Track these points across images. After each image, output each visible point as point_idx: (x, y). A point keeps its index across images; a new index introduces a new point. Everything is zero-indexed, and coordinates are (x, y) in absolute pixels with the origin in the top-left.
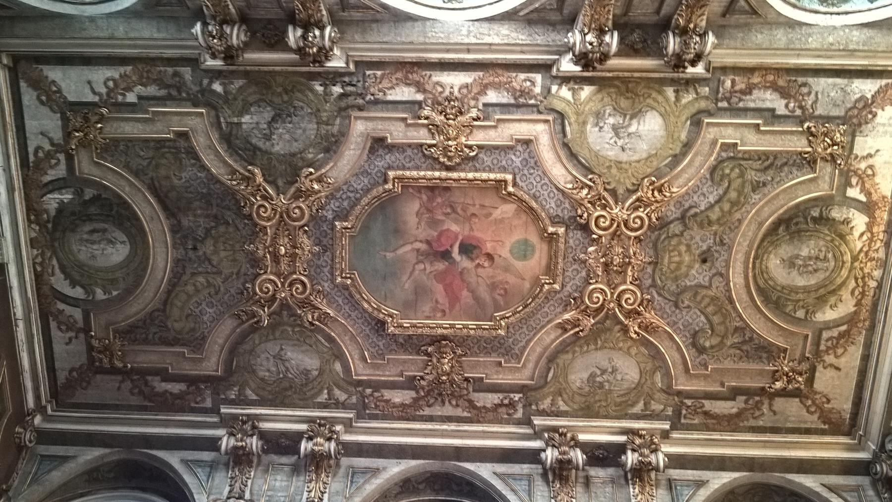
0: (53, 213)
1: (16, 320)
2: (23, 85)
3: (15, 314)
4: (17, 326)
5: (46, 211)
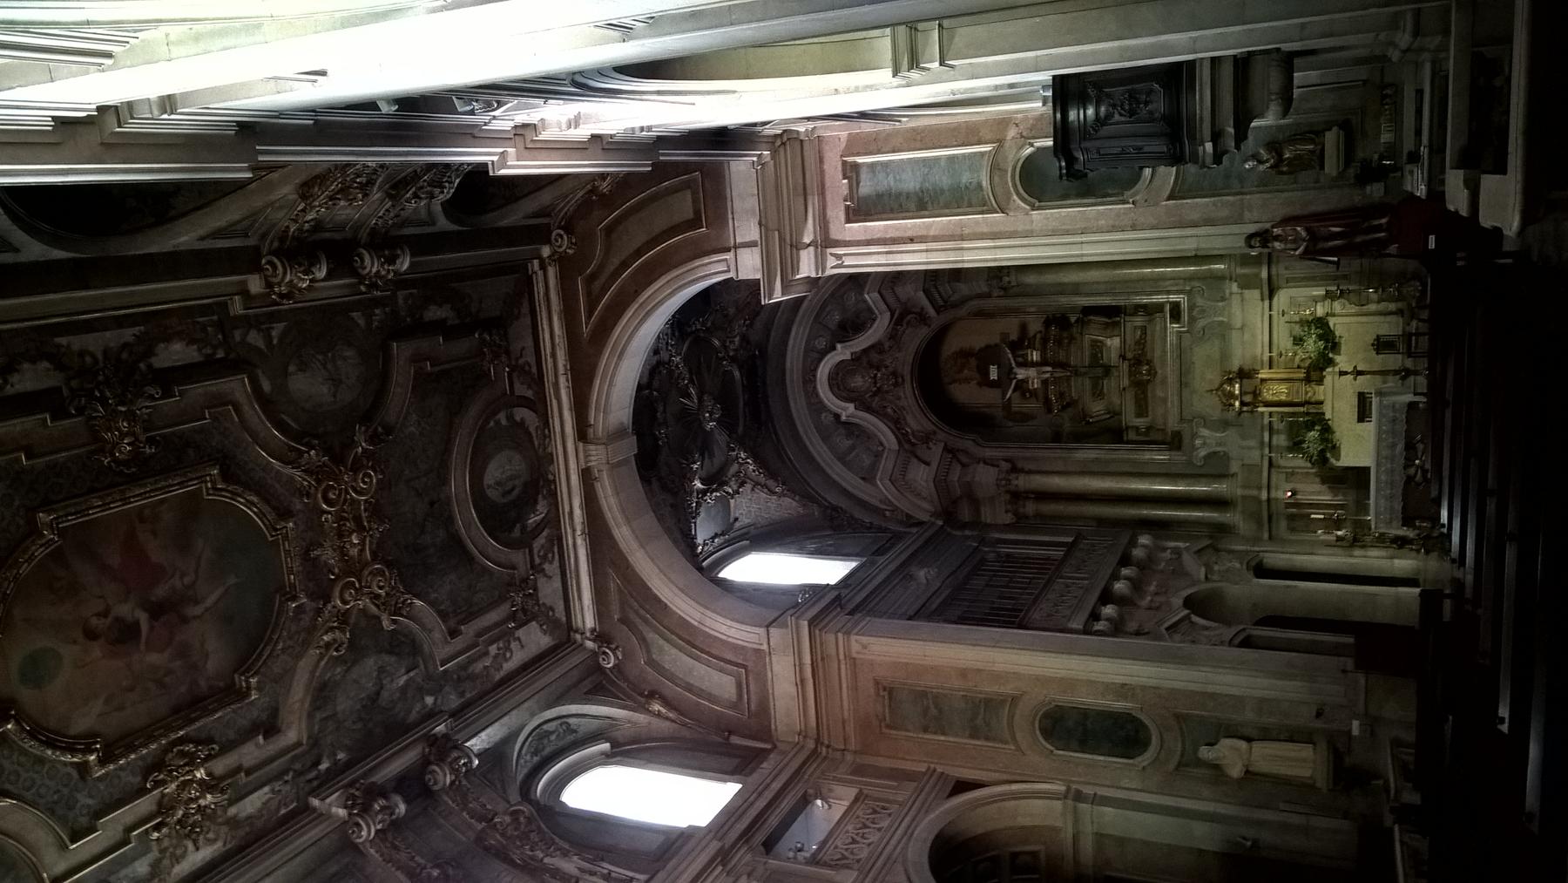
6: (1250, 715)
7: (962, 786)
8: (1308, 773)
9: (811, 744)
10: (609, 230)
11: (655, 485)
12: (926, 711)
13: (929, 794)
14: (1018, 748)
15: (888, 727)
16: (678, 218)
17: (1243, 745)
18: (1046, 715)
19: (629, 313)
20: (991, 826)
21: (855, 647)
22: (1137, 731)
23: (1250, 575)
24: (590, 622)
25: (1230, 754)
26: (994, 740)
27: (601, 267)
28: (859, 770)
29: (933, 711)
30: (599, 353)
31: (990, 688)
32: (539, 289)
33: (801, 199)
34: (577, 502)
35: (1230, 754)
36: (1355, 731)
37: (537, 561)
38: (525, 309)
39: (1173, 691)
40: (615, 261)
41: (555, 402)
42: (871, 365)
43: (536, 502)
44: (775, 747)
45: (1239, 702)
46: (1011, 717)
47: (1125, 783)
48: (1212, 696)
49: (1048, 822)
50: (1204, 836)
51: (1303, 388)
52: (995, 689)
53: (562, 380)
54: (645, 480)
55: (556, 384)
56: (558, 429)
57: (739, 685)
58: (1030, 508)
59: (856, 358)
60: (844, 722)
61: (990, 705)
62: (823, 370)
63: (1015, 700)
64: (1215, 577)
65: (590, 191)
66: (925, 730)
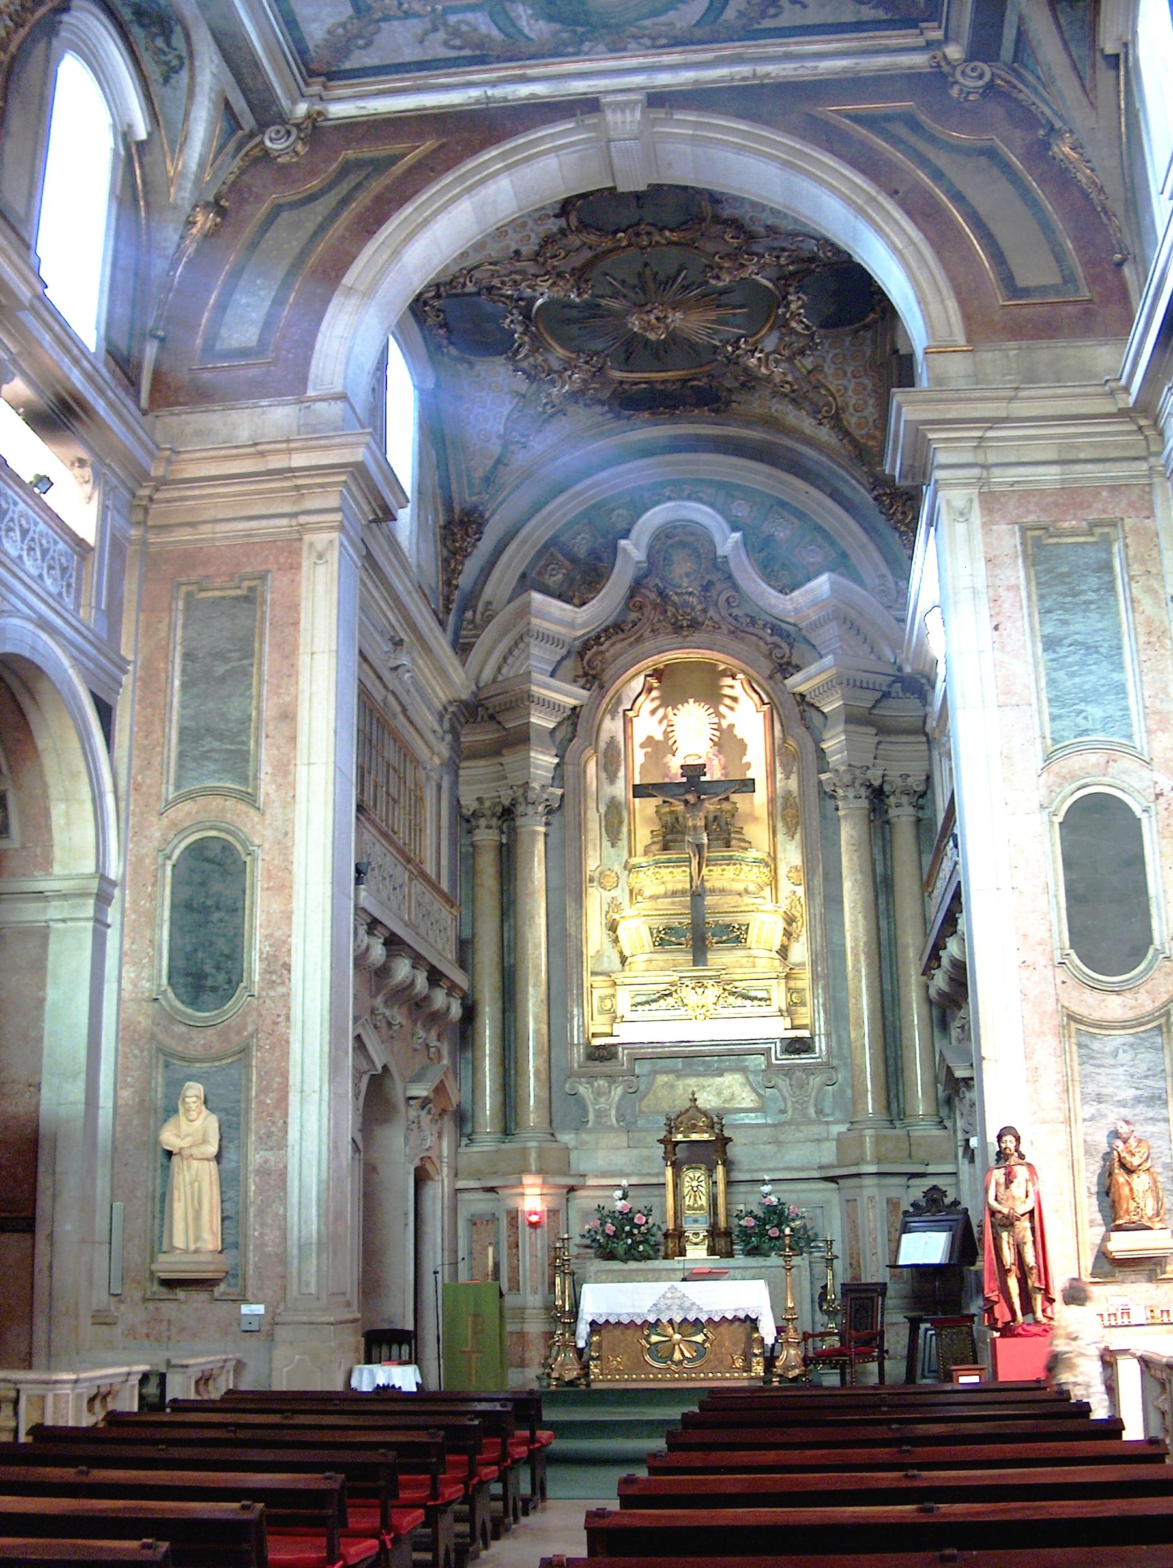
0: (556, 26)
1: (755, 76)
2: (347, 65)
3: (744, 79)
4: (767, 75)
5: (555, 34)
6: (256, 1158)
7: (105, 713)
8: (179, 1241)
9: (156, 471)
10: (990, 153)
11: (553, 225)
12: (221, 656)
13: (98, 665)
14: (169, 804)
15: (189, 595)
16: (1015, 262)
17: (213, 1149)
18: (227, 847)
19: (859, 179)
20: (49, 762)
21: (321, 539)
22: (214, 989)
23: (417, 1163)
24: (340, 110)
25: (193, 1129)
26: (181, 766)
27: (932, 139)
28: (118, 548)
29: (220, 669)
30: (791, 131)
31: (266, 758)
32: (895, 38)
33: (1052, 455)
34: (540, 89)
35: (193, 1129)
36: (245, 1309)
37: (453, 19)
38: (868, 13)
39: (284, 1044)
40: (941, 160)
41: (710, 56)
42: (707, 587)
43: (550, 18)
44: (145, 413)
45: (277, 1139)
46: (225, 794)
47: (129, 973)
48: (283, 1099)
49: (58, 852)
50: (60, 1097)
51: (702, 1228)
52: (266, 768)
53: (744, 70)
54: (566, 207)
55: (739, 60)
56: (666, 59)
57: (243, 353)
58: (487, 836)
59: (719, 565)
60: (192, 525)
61: (239, 763)
62: (701, 513)
63: (250, 799)
64: (413, 1113)
65: (1052, 128)
66: (188, 656)
